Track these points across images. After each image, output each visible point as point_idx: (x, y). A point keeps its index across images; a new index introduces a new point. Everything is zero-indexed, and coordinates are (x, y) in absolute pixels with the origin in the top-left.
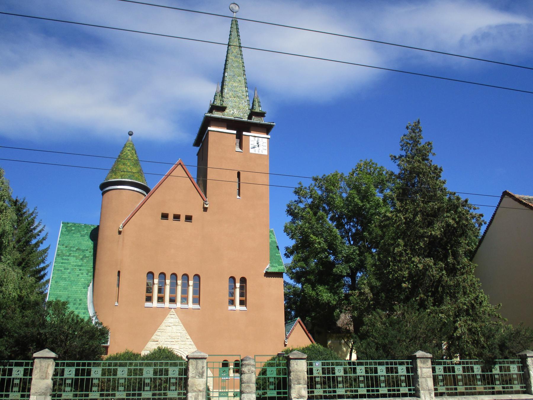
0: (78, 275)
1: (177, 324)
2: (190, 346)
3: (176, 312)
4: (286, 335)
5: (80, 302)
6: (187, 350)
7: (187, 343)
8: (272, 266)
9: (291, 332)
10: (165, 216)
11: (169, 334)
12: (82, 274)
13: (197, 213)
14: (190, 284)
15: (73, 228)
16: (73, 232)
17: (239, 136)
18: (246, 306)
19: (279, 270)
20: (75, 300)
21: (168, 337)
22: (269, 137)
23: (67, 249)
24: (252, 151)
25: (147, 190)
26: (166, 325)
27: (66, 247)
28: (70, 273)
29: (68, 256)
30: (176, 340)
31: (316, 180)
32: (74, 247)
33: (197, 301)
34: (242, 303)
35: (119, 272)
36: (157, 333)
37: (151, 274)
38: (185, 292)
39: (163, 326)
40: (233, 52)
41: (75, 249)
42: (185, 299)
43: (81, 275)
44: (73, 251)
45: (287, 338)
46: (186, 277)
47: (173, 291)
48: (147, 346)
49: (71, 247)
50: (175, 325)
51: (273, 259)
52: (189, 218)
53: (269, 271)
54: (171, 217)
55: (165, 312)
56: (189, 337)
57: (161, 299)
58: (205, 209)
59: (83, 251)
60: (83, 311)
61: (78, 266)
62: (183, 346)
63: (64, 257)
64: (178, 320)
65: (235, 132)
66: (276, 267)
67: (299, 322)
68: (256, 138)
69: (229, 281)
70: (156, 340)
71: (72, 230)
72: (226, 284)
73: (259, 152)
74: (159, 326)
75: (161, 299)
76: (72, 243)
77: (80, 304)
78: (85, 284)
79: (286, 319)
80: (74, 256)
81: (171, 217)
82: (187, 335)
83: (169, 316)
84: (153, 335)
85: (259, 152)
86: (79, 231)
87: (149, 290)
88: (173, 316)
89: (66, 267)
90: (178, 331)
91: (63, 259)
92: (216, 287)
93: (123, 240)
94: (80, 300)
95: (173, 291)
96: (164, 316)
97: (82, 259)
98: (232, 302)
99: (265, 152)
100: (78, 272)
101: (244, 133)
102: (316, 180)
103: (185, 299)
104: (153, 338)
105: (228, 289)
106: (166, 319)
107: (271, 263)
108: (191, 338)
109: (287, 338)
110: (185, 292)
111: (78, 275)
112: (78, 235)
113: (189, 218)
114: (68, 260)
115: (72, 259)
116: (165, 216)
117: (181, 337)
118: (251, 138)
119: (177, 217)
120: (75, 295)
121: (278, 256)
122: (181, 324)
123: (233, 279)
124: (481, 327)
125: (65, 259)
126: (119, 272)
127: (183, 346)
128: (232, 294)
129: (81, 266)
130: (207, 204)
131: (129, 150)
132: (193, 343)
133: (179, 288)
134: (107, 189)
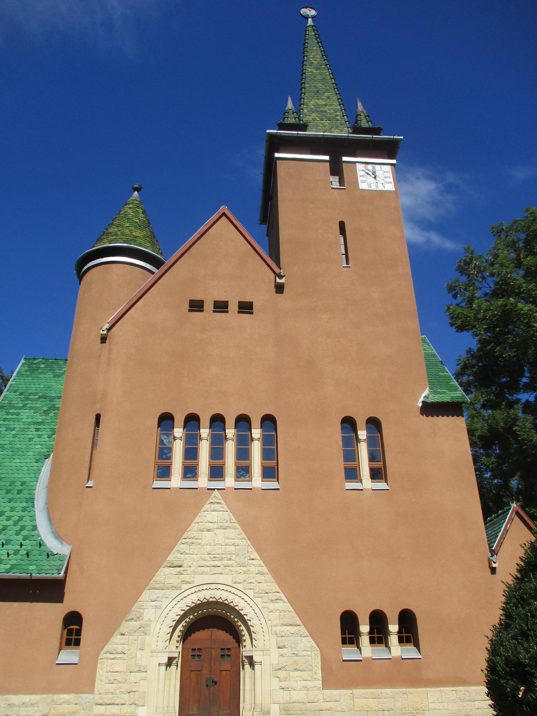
0: (30, 439)
1: (225, 525)
2: (259, 578)
3: (224, 499)
4: (490, 547)
5: (21, 488)
6: (249, 586)
7: (253, 568)
8: (435, 393)
9: (503, 537)
10: (196, 306)
11: (208, 548)
12: (40, 436)
13: (261, 295)
14: (254, 436)
15: (42, 366)
16: (40, 371)
17: (336, 169)
18: (386, 481)
19: (452, 398)
20: (12, 484)
21: (206, 556)
22: (394, 161)
23: (22, 396)
24: (363, 186)
25: (157, 263)
26: (201, 526)
27: (21, 394)
28: (14, 436)
29: (20, 408)
30: (225, 562)
31: (498, 232)
32: (35, 394)
33: (269, 473)
34: (377, 474)
35: (98, 417)
36: (179, 547)
37: (166, 420)
38: (243, 453)
39: (193, 531)
40: (312, 63)
41: (37, 397)
42: (243, 471)
43: (37, 439)
44: (32, 400)
45: (493, 553)
46: (243, 421)
47: (217, 453)
48: (156, 578)
49: (30, 394)
50: (220, 528)
51: (435, 381)
52: (246, 307)
53: (430, 400)
54: (209, 306)
55: (197, 500)
56: (255, 555)
57: (190, 472)
58: (280, 289)
59: (52, 399)
60: (24, 504)
61: (35, 423)
62: (241, 577)
63: (13, 411)
64: (227, 515)
65: (327, 158)
66: (444, 393)
67: (517, 514)
68: (370, 167)
69: (342, 428)
70: (176, 563)
71: (39, 368)
72: (336, 433)
73: (377, 186)
74: (185, 531)
75: (190, 472)
76: (33, 388)
77: (20, 492)
78: (40, 453)
79: (487, 512)
80: (31, 408)
81: (209, 306)
82: (251, 549)
83: (207, 506)
84: (170, 550)
85: (377, 186)
86: (52, 370)
87: (164, 453)
88: (217, 506)
89: (12, 426)
90: (228, 541)
91: (8, 413)
92: (311, 442)
93: (110, 354)
94: (23, 484)
95: (217, 453)
96: (197, 508)
97: (46, 412)
98: (352, 474)
99: (390, 187)
100: (32, 433)
101: (345, 159)
102: (498, 232)
103: (243, 471)
104: (171, 557)
105: (341, 443)
106: (202, 513)
107: (431, 388)
108: (262, 558)
109: (493, 553)
110: (243, 453)
111: (30, 439)
112: (50, 374)
113: (246, 307)
114: (18, 414)
115: (26, 415)
116: (196, 306)
117: (237, 555)
118: (359, 167)
119: (221, 307)
120: (15, 475)
121: (446, 377)
122: (237, 525)
123: (349, 423)
124: (530, 611)
125: (13, 414)
126: (98, 417)
127: (241, 577)
128: (350, 455)
129: (40, 423)
130: (281, 277)
131: (130, 208)
132: (265, 569)
133: (230, 448)
134: (86, 268)
